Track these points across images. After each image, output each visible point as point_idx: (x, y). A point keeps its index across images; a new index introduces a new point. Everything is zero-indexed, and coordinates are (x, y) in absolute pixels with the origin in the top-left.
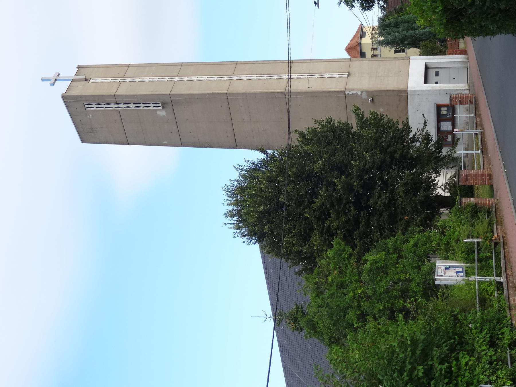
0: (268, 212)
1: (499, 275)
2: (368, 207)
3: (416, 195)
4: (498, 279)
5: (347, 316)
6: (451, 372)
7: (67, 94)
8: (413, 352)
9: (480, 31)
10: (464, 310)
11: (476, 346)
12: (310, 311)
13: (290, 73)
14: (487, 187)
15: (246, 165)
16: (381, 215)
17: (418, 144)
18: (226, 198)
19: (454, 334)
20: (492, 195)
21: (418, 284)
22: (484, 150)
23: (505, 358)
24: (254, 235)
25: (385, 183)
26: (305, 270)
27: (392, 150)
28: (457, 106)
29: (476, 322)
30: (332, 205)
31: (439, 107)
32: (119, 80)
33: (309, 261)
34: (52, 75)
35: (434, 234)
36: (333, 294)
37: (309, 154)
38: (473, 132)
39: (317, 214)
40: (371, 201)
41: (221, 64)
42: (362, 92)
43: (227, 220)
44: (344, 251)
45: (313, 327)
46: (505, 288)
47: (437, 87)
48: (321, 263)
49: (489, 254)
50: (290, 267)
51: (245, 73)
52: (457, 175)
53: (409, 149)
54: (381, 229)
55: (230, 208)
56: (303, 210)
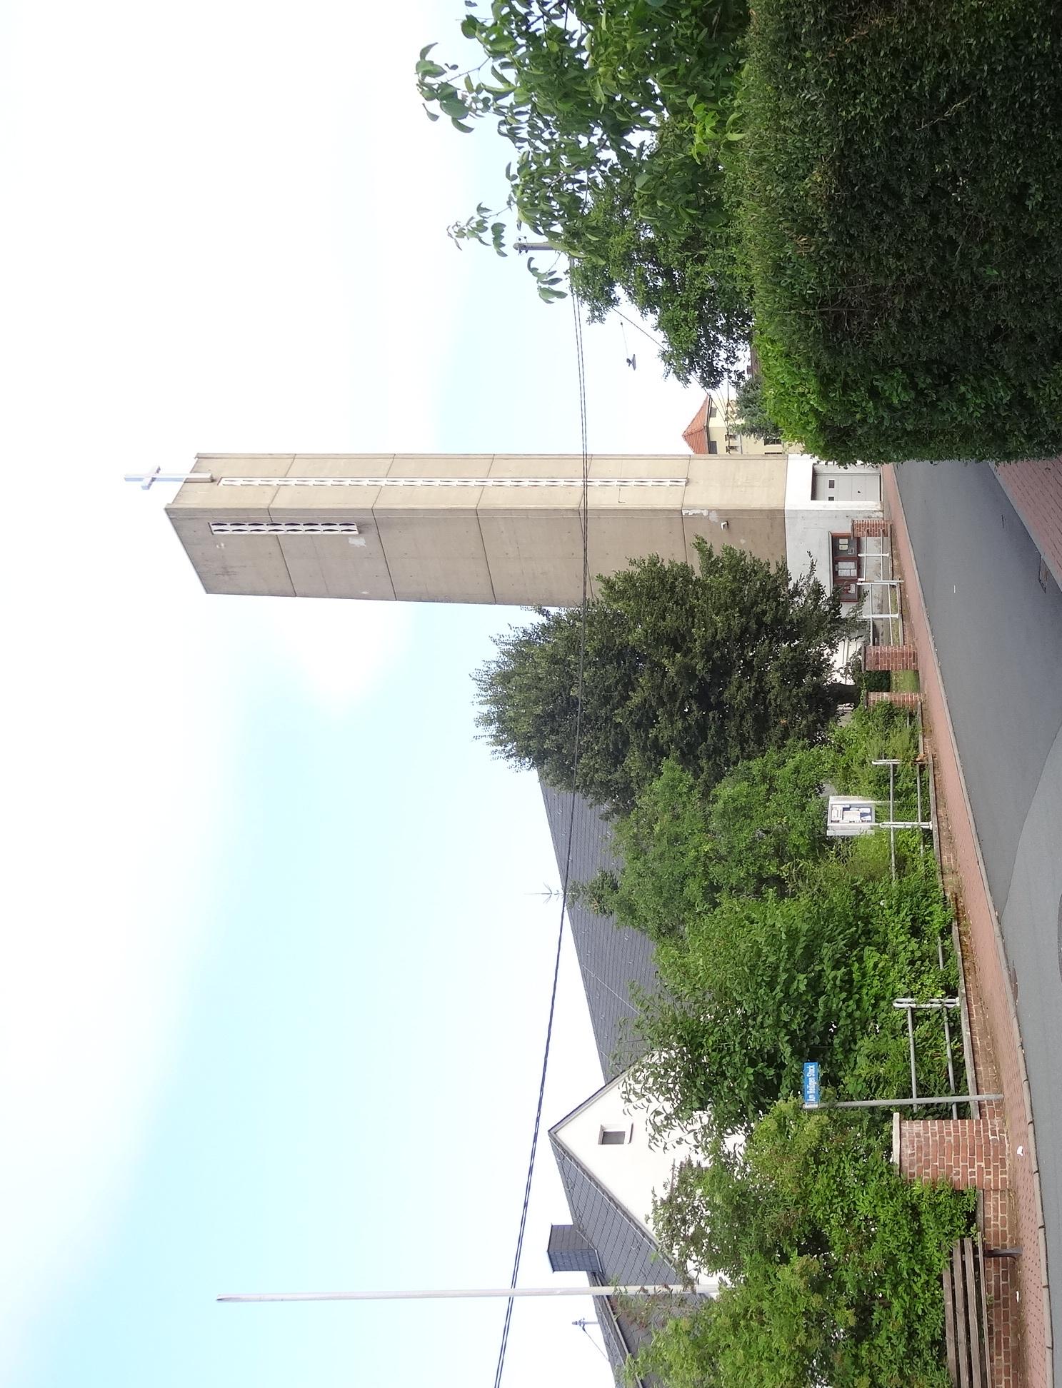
0: (551, 716)
1: (926, 818)
2: (720, 705)
3: (800, 685)
4: (926, 825)
5: (686, 889)
6: (851, 981)
7: (176, 506)
8: (791, 953)
9: (876, 458)
10: (872, 878)
11: (891, 936)
12: (625, 883)
13: (585, 477)
14: (910, 674)
15: (512, 635)
16: (742, 717)
17: (801, 601)
18: (477, 691)
19: (857, 918)
20: (917, 688)
21: (802, 834)
22: (904, 614)
23: (935, 952)
24: (528, 754)
25: (748, 664)
26: (617, 811)
27: (759, 610)
28: (864, 539)
29: (890, 897)
30: (661, 703)
31: (835, 539)
32: (275, 482)
33: (623, 796)
34: (147, 471)
35: (827, 754)
36: (662, 854)
37: (621, 616)
38: (888, 583)
39: (635, 718)
40: (726, 695)
41: (466, 457)
42: (710, 511)
43: (481, 730)
44: (681, 781)
45: (630, 909)
46: (936, 839)
47: (832, 505)
48: (643, 801)
49: (910, 785)
50: (591, 806)
51: (508, 475)
52: (864, 651)
53: (787, 608)
54: (743, 740)
55: (485, 709)
56: (612, 710)
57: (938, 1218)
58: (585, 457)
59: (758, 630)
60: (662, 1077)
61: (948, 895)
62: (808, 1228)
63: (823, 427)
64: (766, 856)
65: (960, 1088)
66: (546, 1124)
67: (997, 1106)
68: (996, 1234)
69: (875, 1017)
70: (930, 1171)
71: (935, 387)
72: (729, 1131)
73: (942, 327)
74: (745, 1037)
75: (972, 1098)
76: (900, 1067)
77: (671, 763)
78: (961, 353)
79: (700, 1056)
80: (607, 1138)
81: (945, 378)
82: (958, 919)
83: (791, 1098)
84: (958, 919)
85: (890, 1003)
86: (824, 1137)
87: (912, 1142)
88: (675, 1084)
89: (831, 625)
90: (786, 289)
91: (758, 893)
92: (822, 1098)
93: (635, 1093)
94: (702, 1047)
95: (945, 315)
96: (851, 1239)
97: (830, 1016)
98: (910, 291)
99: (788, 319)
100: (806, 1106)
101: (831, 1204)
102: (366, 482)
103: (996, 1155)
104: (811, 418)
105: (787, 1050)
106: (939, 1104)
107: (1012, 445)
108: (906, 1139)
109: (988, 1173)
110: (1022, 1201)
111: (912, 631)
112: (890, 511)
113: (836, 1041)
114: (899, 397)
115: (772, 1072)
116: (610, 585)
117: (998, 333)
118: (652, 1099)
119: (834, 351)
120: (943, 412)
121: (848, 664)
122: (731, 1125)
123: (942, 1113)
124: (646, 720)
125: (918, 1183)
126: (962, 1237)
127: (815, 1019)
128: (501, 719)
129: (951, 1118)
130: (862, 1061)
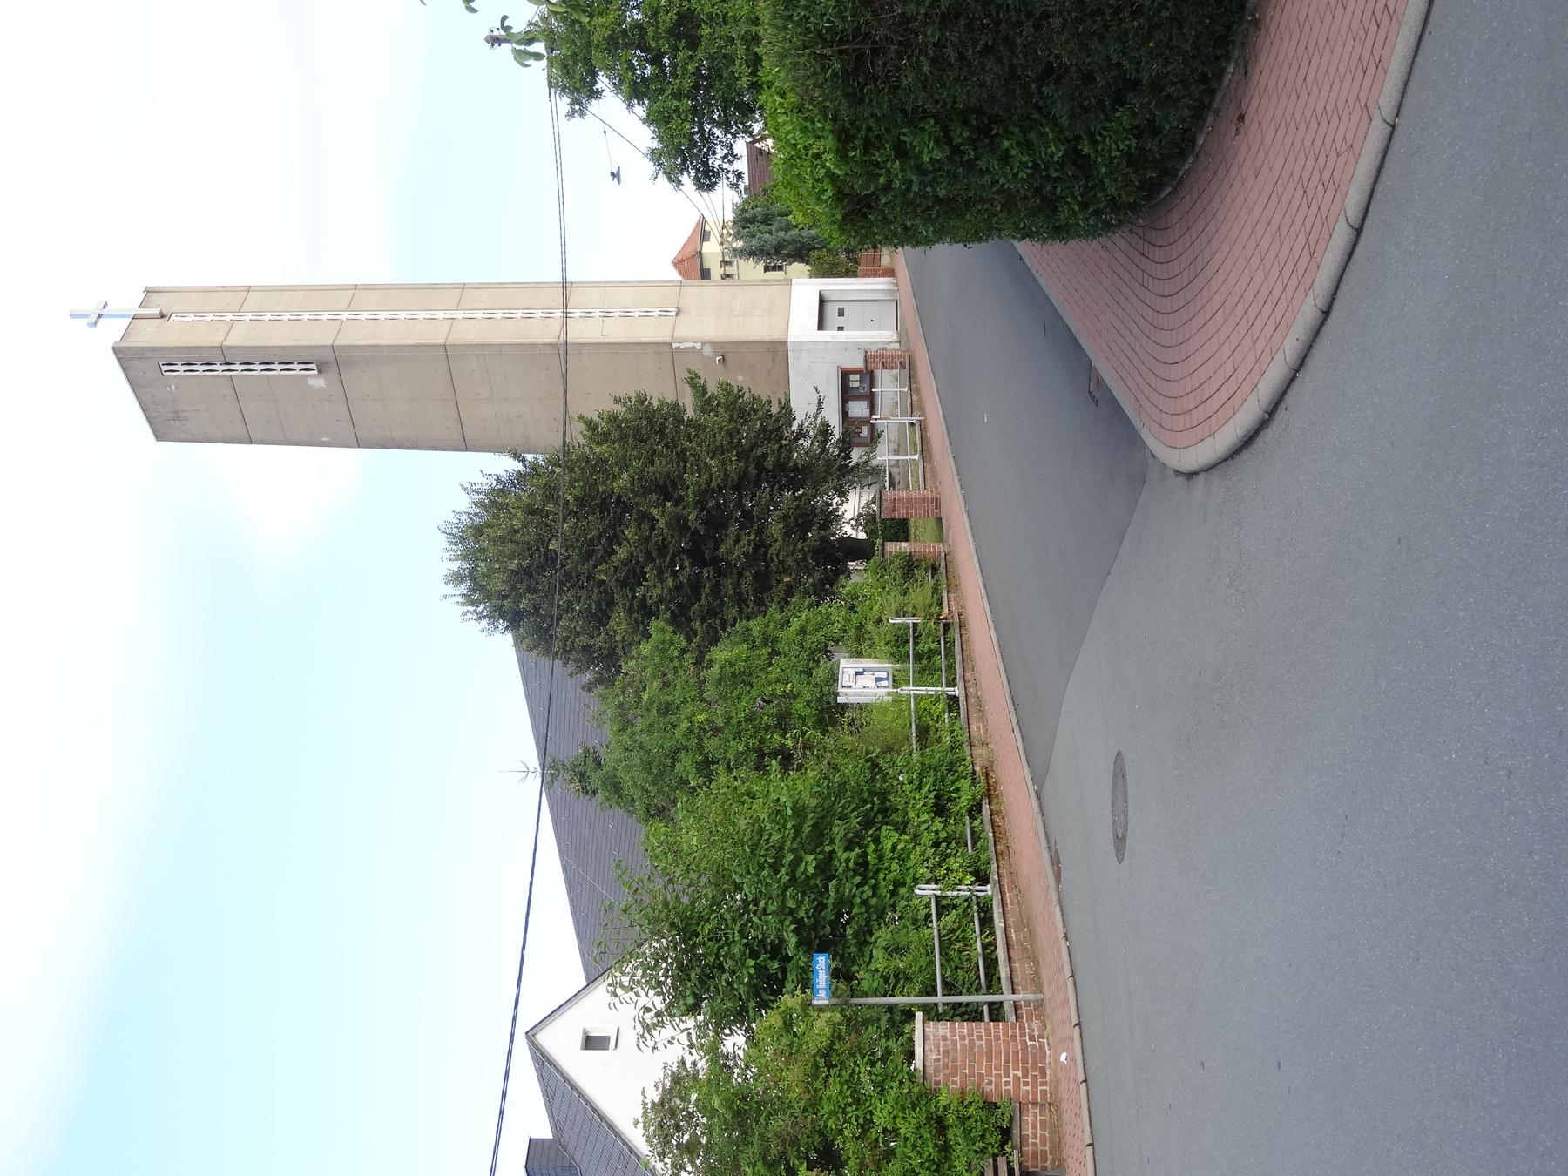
1: (952, 683)
2: (715, 560)
3: (805, 538)
4: (951, 691)
6: (865, 864)
8: (797, 831)
10: (890, 750)
11: (911, 815)
12: (609, 758)
13: (565, 305)
14: (932, 522)
15: (484, 483)
16: (740, 575)
17: (807, 443)
18: (446, 545)
19: (872, 793)
20: (940, 537)
21: (808, 703)
22: (925, 454)
23: (963, 834)
24: (502, 615)
25: (747, 515)
26: (600, 680)
28: (878, 373)
30: (649, 558)
31: (845, 375)
32: (229, 317)
33: (607, 662)
34: (93, 307)
35: (835, 611)
36: (651, 725)
37: (605, 461)
38: (906, 420)
39: (621, 575)
40: (722, 549)
41: (434, 287)
42: (703, 344)
46: (962, 707)
48: (629, 666)
49: (933, 646)
50: (571, 675)
51: (481, 306)
52: (878, 499)
53: (790, 451)
54: (741, 600)
55: (455, 566)
56: (595, 566)
57: (967, 1132)
58: (565, 285)
59: (758, 475)
60: (652, 969)
61: (977, 769)
62: (817, 1139)
63: (840, 196)
64: (767, 728)
65: (992, 984)
66: (524, 1025)
67: (1036, 1008)
68: (1035, 1155)
69: (894, 906)
70: (958, 1079)
71: (972, 142)
72: (727, 1031)
73: (983, 65)
74: (745, 925)
75: (1006, 997)
76: (923, 962)
77: (661, 624)
78: (1004, 100)
79: (695, 946)
80: (590, 1042)
81: (985, 131)
82: (989, 796)
83: (798, 992)
84: (989, 796)
85: (911, 889)
86: (836, 1037)
87: (937, 1046)
88: (667, 977)
89: (843, 475)
90: (798, 24)
91: (760, 767)
92: (834, 993)
93: (622, 987)
94: (697, 935)
95: (987, 50)
96: (868, 1154)
97: (843, 903)
98: (946, 20)
99: (802, 61)
100: (815, 1002)
101: (844, 1113)
102: (325, 316)
103: (1035, 1063)
104: (827, 185)
105: (792, 940)
106: (968, 1004)
107: (1064, 214)
108: (930, 1041)
109: (1026, 1084)
110: (1066, 1117)
111: (934, 475)
112: (908, 341)
113: (849, 931)
114: (931, 153)
115: (776, 965)
116: (591, 426)
117: (1050, 73)
118: (641, 992)
119: (855, 99)
120: (982, 173)
121: (860, 515)
122: (730, 1025)
123: (971, 1014)
124: (633, 576)
125: (944, 1092)
126: (995, 1156)
127: (825, 906)
128: (472, 577)
129: (982, 1020)
130: (879, 954)
